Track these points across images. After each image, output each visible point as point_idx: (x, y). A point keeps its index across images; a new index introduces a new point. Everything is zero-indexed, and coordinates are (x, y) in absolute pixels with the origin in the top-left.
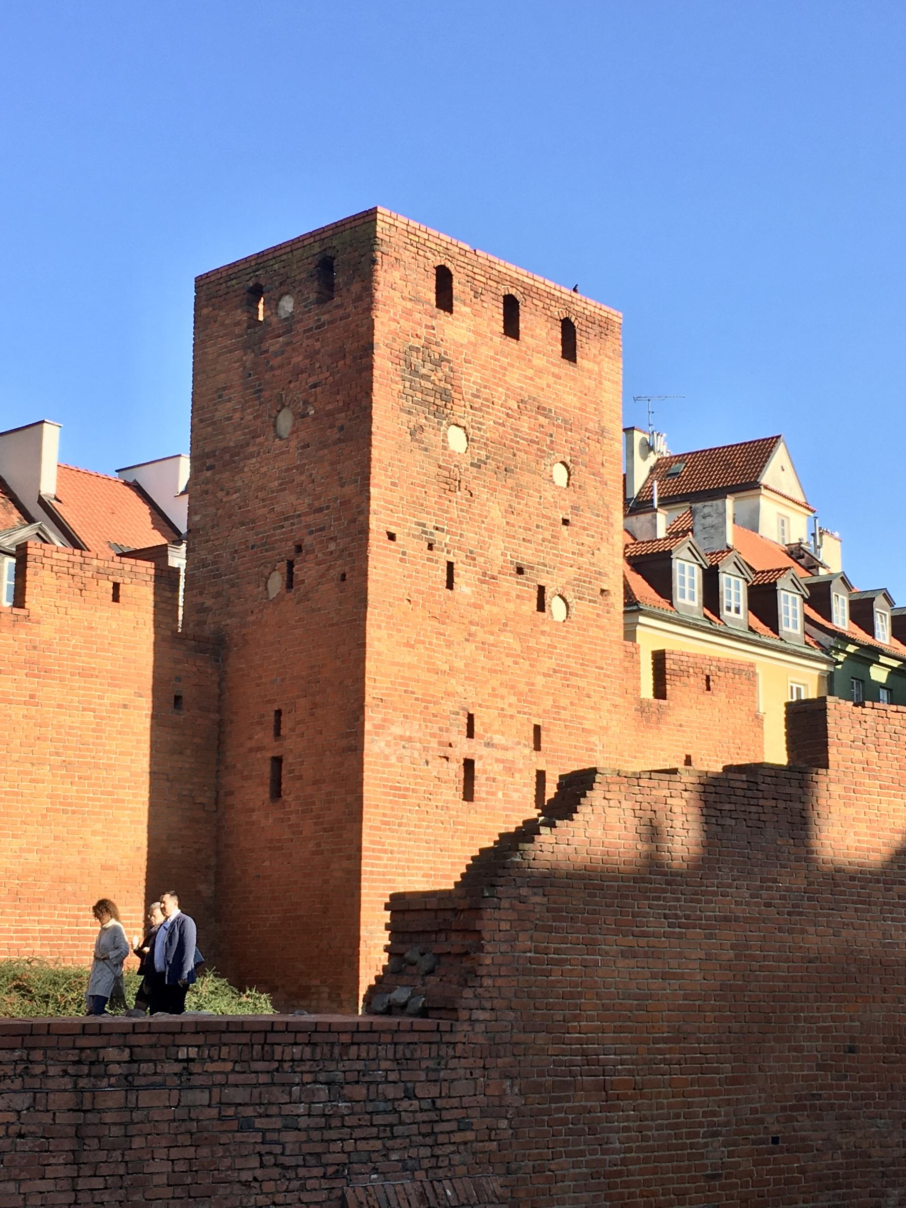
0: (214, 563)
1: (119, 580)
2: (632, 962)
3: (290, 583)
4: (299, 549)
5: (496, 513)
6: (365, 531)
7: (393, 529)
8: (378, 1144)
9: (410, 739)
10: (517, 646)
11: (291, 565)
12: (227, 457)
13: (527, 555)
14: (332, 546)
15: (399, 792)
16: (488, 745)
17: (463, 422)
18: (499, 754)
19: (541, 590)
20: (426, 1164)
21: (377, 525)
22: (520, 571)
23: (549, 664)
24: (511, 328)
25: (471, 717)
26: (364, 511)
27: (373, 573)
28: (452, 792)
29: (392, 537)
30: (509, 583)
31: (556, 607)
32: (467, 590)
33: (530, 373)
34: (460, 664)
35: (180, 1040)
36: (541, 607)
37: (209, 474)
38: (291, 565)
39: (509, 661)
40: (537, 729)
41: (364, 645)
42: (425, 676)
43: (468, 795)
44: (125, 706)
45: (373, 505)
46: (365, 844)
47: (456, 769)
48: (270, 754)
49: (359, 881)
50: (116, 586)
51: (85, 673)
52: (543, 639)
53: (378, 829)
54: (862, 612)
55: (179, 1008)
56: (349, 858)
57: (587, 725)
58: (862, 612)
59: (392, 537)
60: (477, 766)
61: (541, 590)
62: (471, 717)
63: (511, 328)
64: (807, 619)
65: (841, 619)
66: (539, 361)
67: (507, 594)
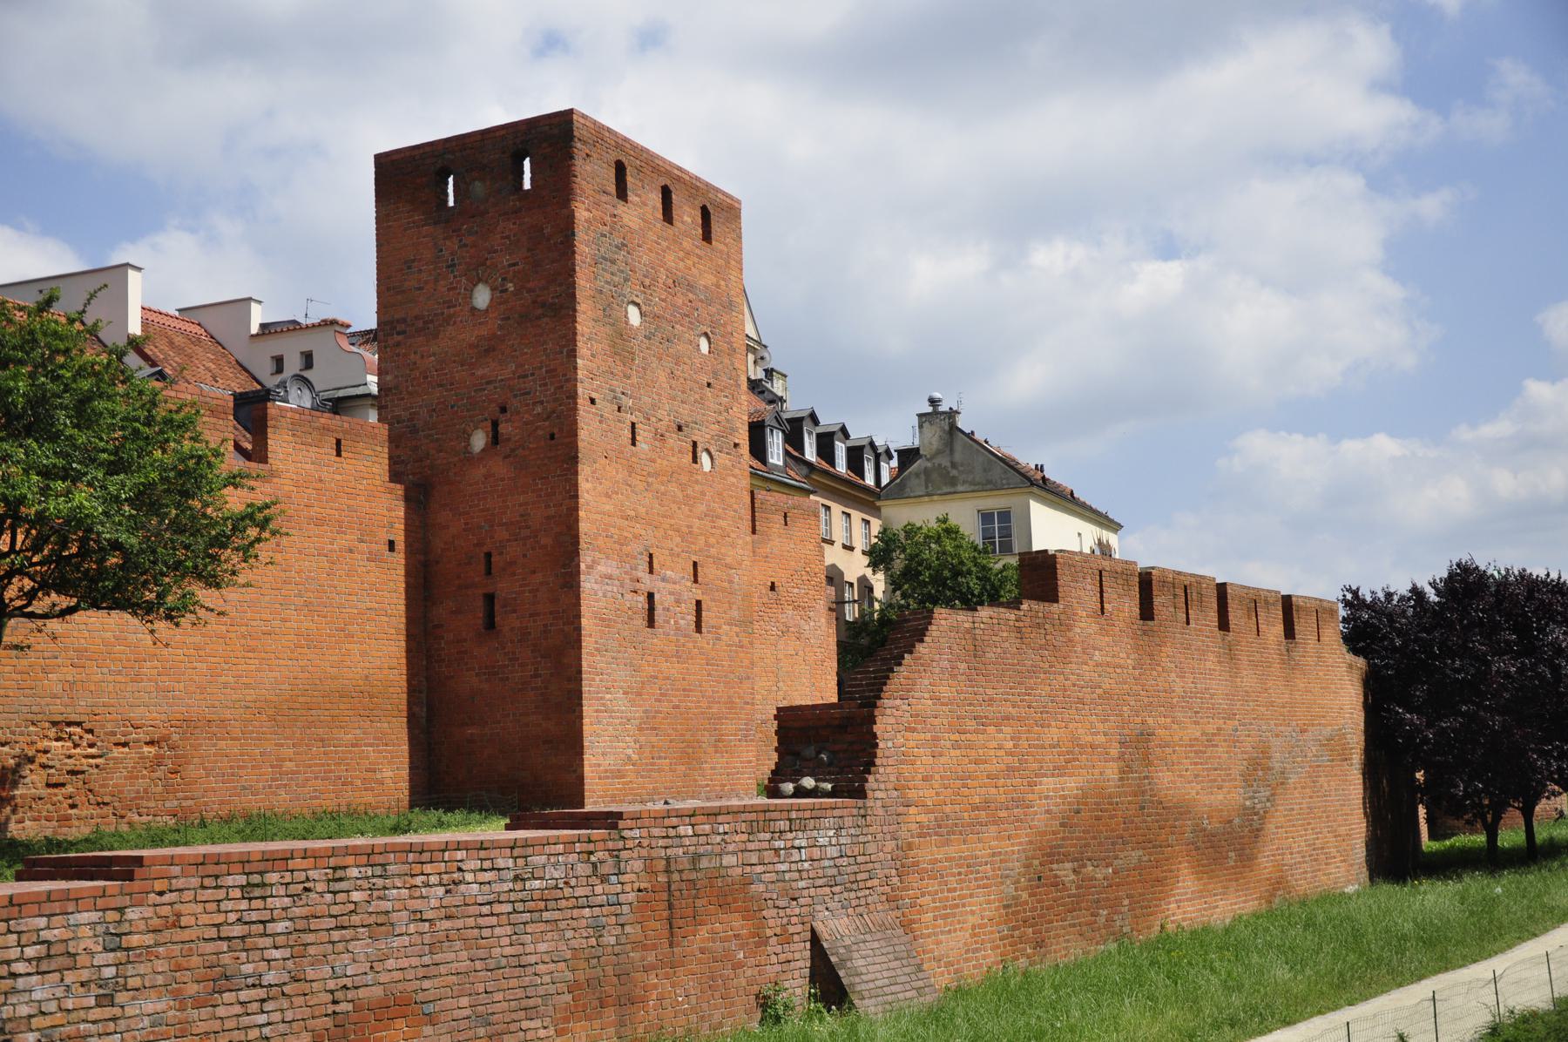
0: (411, 420)
1: (340, 436)
2: (958, 752)
3: (495, 439)
4: (503, 410)
5: (662, 377)
6: (573, 396)
7: (594, 395)
8: (827, 890)
9: (610, 577)
10: (680, 495)
11: (495, 424)
12: (420, 324)
13: (685, 414)
14: (539, 409)
15: (604, 621)
16: (663, 580)
17: (637, 300)
18: (669, 586)
19: (695, 444)
20: (854, 903)
21: (582, 391)
22: (680, 428)
23: (702, 508)
24: (668, 216)
25: (651, 556)
26: (573, 380)
27: (583, 434)
28: (640, 622)
29: (593, 401)
30: (673, 440)
31: (705, 459)
32: (645, 446)
33: (681, 254)
34: (642, 510)
35: (720, 819)
36: (695, 460)
37: (400, 338)
38: (495, 424)
39: (674, 507)
40: (695, 564)
41: (576, 497)
42: (620, 522)
43: (651, 622)
44: (351, 551)
45: (581, 374)
46: (584, 669)
47: (642, 600)
48: (481, 591)
49: (581, 698)
50: (338, 442)
51: (319, 522)
52: (697, 487)
53: (592, 655)
54: (825, 445)
55: (582, 806)
56: (569, 680)
57: (728, 560)
58: (825, 445)
59: (593, 401)
60: (657, 597)
61: (695, 444)
62: (651, 556)
63: (668, 216)
64: (787, 453)
65: (810, 454)
66: (687, 244)
67: (672, 449)
